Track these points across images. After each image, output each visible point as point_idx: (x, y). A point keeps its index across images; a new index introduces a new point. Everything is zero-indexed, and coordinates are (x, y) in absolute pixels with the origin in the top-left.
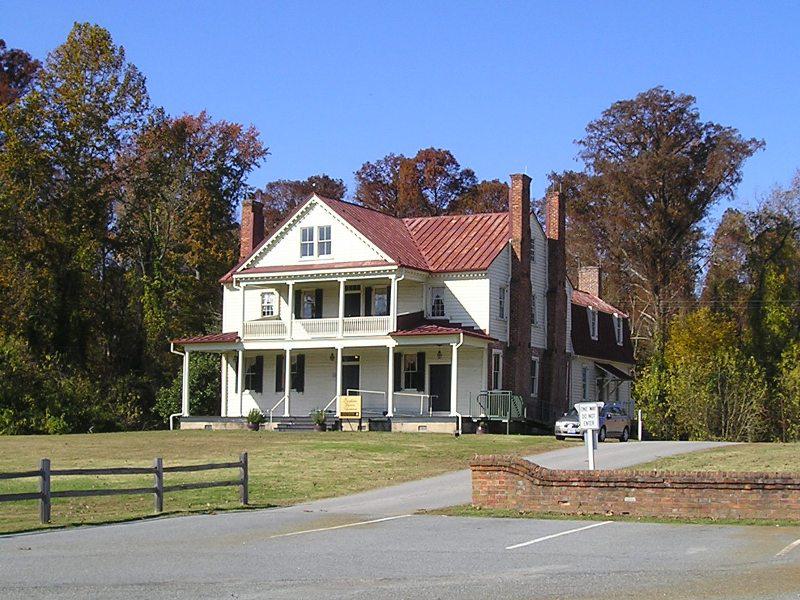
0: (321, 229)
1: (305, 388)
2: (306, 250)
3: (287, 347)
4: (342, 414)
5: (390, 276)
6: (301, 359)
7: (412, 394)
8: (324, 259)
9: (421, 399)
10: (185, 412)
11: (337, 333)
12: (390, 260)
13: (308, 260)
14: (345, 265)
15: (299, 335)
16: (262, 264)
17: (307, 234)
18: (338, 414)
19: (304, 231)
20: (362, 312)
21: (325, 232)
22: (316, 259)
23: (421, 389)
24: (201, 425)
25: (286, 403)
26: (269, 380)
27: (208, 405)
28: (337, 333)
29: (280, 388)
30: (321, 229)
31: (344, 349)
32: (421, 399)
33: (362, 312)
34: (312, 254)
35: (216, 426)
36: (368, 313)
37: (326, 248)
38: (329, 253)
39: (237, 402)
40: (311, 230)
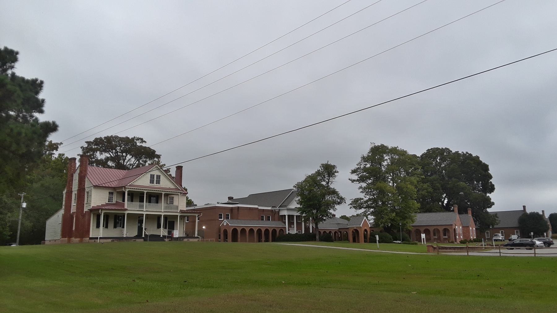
0: (157, 176)
2: (152, 181)
16: (172, 187)
17: (152, 176)
21: (158, 177)
30: (157, 176)
34: (153, 183)
37: (158, 182)
40: (154, 175)
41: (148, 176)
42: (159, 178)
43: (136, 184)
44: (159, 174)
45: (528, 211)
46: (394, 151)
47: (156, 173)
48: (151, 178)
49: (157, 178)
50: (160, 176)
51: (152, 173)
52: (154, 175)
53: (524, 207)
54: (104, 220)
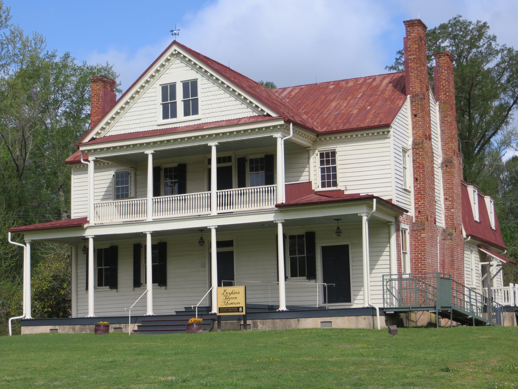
0: (185, 85)
1: (168, 280)
2: (169, 111)
3: (147, 229)
4: (220, 310)
5: (275, 135)
6: (163, 244)
7: (302, 282)
8: (192, 120)
9: (313, 291)
10: (27, 314)
11: (206, 210)
12: (273, 115)
13: (170, 123)
14: (217, 125)
15: (154, 215)
16: (249, 113)
17: (168, 91)
18: (215, 310)
19: (164, 88)
20: (235, 180)
21: (191, 88)
22: (181, 119)
23: (312, 276)
24: (45, 329)
25: (150, 301)
26: (125, 274)
27: (54, 306)
28: (206, 210)
29: (138, 282)
30: (185, 85)
31: (220, 229)
32: (313, 291)
33: (235, 180)
34: (174, 115)
35: (63, 330)
36: (242, 184)
37: (192, 107)
38: (196, 112)
39: (90, 301)
40: (173, 86)
41: (154, 96)
42: (195, 93)
43: (114, 130)
44: (190, 74)
45: (461, 19)
46: (194, 332)
47: (178, 73)
48: (164, 98)
49: (186, 94)
50: (194, 83)
51: (166, 78)
52: (173, 86)
53: (488, 27)
54: (446, 181)
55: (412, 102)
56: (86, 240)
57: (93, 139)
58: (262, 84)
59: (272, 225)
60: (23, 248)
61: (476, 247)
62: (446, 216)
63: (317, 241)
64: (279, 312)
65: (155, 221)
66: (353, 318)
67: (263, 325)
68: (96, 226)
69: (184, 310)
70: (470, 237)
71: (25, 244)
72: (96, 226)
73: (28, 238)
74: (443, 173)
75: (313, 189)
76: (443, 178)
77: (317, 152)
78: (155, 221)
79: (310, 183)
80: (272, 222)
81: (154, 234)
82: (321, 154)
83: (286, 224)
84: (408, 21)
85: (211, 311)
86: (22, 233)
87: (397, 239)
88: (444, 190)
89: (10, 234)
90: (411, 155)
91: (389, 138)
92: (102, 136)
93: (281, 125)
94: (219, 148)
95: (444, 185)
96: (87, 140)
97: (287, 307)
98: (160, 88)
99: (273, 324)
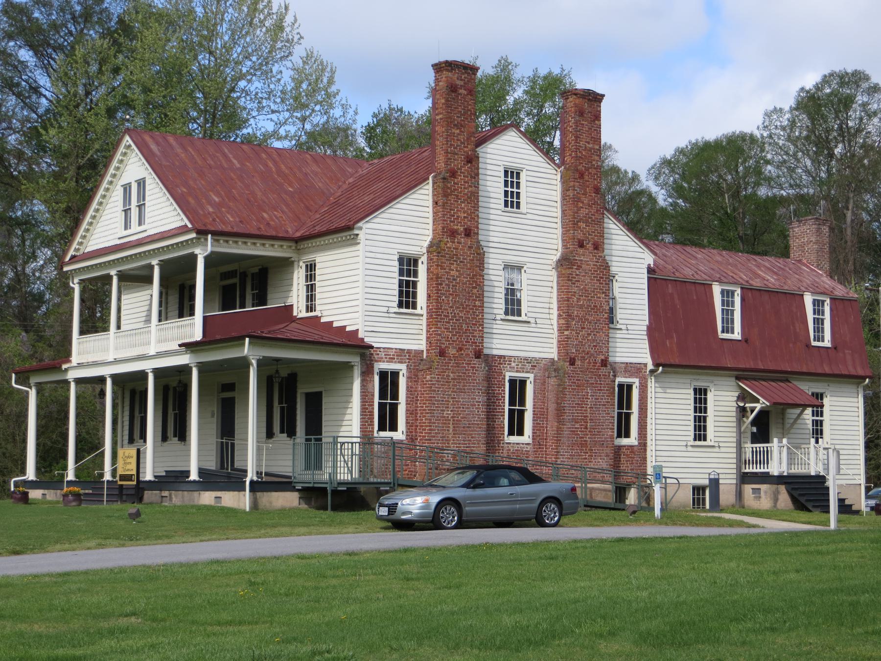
40: (130, 184)
52: (130, 184)
55: (434, 183)
56: (67, 382)
57: (73, 257)
58: (847, 74)
59: (184, 370)
60: (27, 392)
61: (734, 379)
62: (559, 341)
63: (299, 385)
64: (191, 482)
65: (116, 362)
66: (236, 493)
67: (177, 498)
68: (80, 365)
69: (164, 474)
70: (661, 368)
71: (30, 388)
72: (80, 365)
73: (33, 380)
74: (558, 277)
75: (295, 314)
76: (558, 283)
77: (301, 264)
78: (159, 355)
79: (291, 307)
80: (187, 365)
81: (157, 372)
82: (307, 266)
83: (202, 367)
84: (440, 63)
85: (188, 477)
86: (26, 375)
87: (364, 386)
88: (558, 301)
89: (13, 375)
90: (425, 262)
91: (359, 243)
92: (81, 252)
93: (192, 239)
94: (163, 265)
95: (558, 295)
96: (67, 259)
97: (155, 477)
98: (122, 189)
99: (183, 497)
